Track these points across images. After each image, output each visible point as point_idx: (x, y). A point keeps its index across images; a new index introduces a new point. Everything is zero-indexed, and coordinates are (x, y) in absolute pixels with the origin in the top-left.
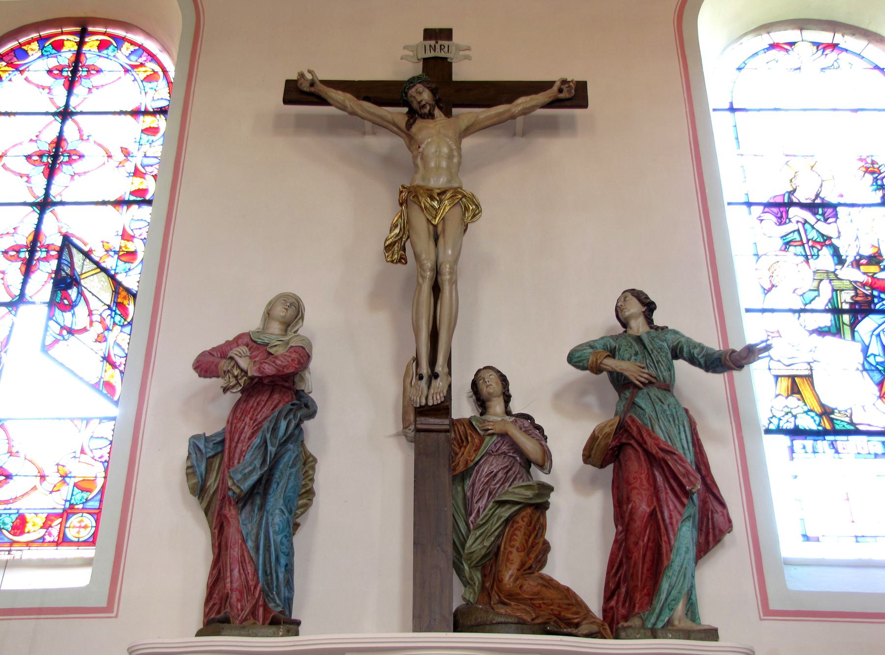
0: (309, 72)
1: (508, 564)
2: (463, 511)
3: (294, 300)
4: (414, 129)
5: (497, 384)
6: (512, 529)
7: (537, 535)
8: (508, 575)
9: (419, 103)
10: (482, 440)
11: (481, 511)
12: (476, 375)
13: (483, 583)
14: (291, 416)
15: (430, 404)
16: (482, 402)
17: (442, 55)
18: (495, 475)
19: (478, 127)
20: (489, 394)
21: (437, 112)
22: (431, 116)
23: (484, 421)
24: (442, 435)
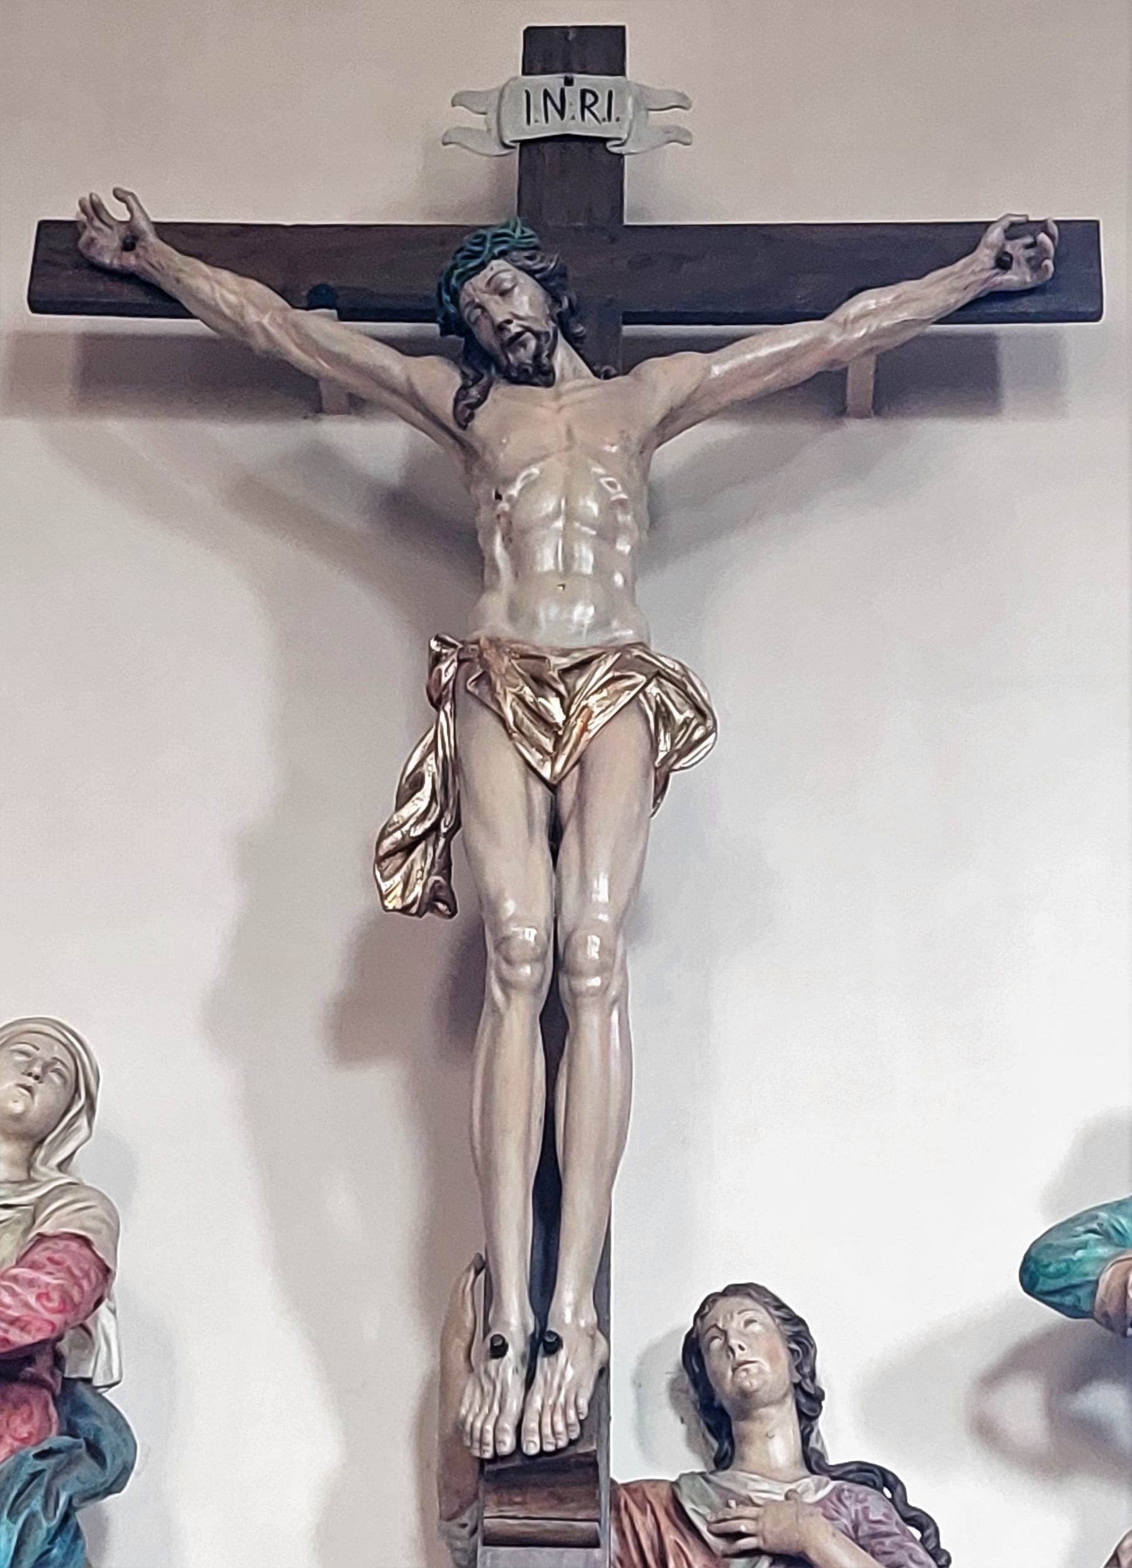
0: (120, 195)
3: (59, 1052)
4: (483, 422)
5: (772, 1358)
9: (500, 328)
12: (700, 1315)
14: (36, 1504)
15: (532, 1449)
17: (589, 127)
19: (706, 408)
20: (745, 1394)
21: (564, 358)
22: (540, 374)
23: (726, 1494)
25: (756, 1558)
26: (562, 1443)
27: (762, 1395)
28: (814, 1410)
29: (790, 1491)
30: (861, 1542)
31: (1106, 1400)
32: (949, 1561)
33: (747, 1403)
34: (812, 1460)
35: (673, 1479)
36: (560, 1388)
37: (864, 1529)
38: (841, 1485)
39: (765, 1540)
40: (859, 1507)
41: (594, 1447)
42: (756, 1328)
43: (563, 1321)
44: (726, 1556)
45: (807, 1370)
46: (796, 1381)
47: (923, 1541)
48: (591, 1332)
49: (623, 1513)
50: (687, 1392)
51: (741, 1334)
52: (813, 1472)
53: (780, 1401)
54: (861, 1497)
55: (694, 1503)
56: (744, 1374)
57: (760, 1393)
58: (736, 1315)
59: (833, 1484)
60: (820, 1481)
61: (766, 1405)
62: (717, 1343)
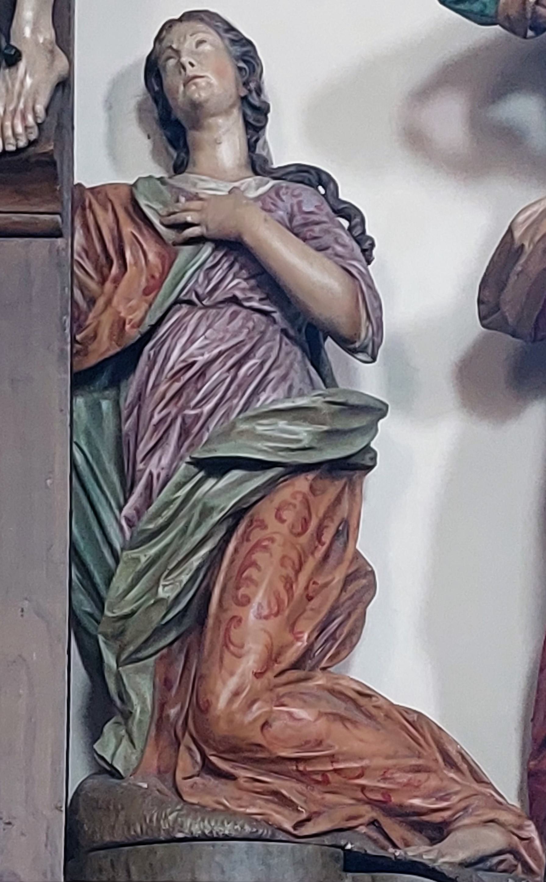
1: (227, 657)
2: (115, 478)
5: (220, 73)
6: (248, 546)
7: (326, 556)
8: (232, 685)
10: (168, 262)
11: (156, 486)
12: (158, 39)
13: (162, 706)
16: (174, 128)
18: (202, 373)
24: (40, 245)
25: (201, 245)
26: (22, 143)
27: (210, 106)
28: (258, 121)
29: (234, 188)
30: (296, 231)
31: (521, 108)
32: (373, 245)
33: (197, 111)
34: (257, 165)
35: (132, 182)
36: (19, 96)
37: (298, 220)
38: (279, 184)
39: (207, 228)
40: (295, 200)
41: (51, 148)
42: (206, 47)
43: (25, 38)
44: (175, 244)
45: (252, 85)
46: (243, 95)
47: (350, 229)
48: (50, 47)
49: (88, 211)
50: (151, 112)
51: (192, 53)
52: (256, 173)
53: (227, 112)
54: (296, 193)
55: (148, 199)
56: (194, 87)
57: (208, 104)
58: (188, 37)
59: (272, 183)
60: (261, 180)
61: (213, 115)
62: (172, 62)
